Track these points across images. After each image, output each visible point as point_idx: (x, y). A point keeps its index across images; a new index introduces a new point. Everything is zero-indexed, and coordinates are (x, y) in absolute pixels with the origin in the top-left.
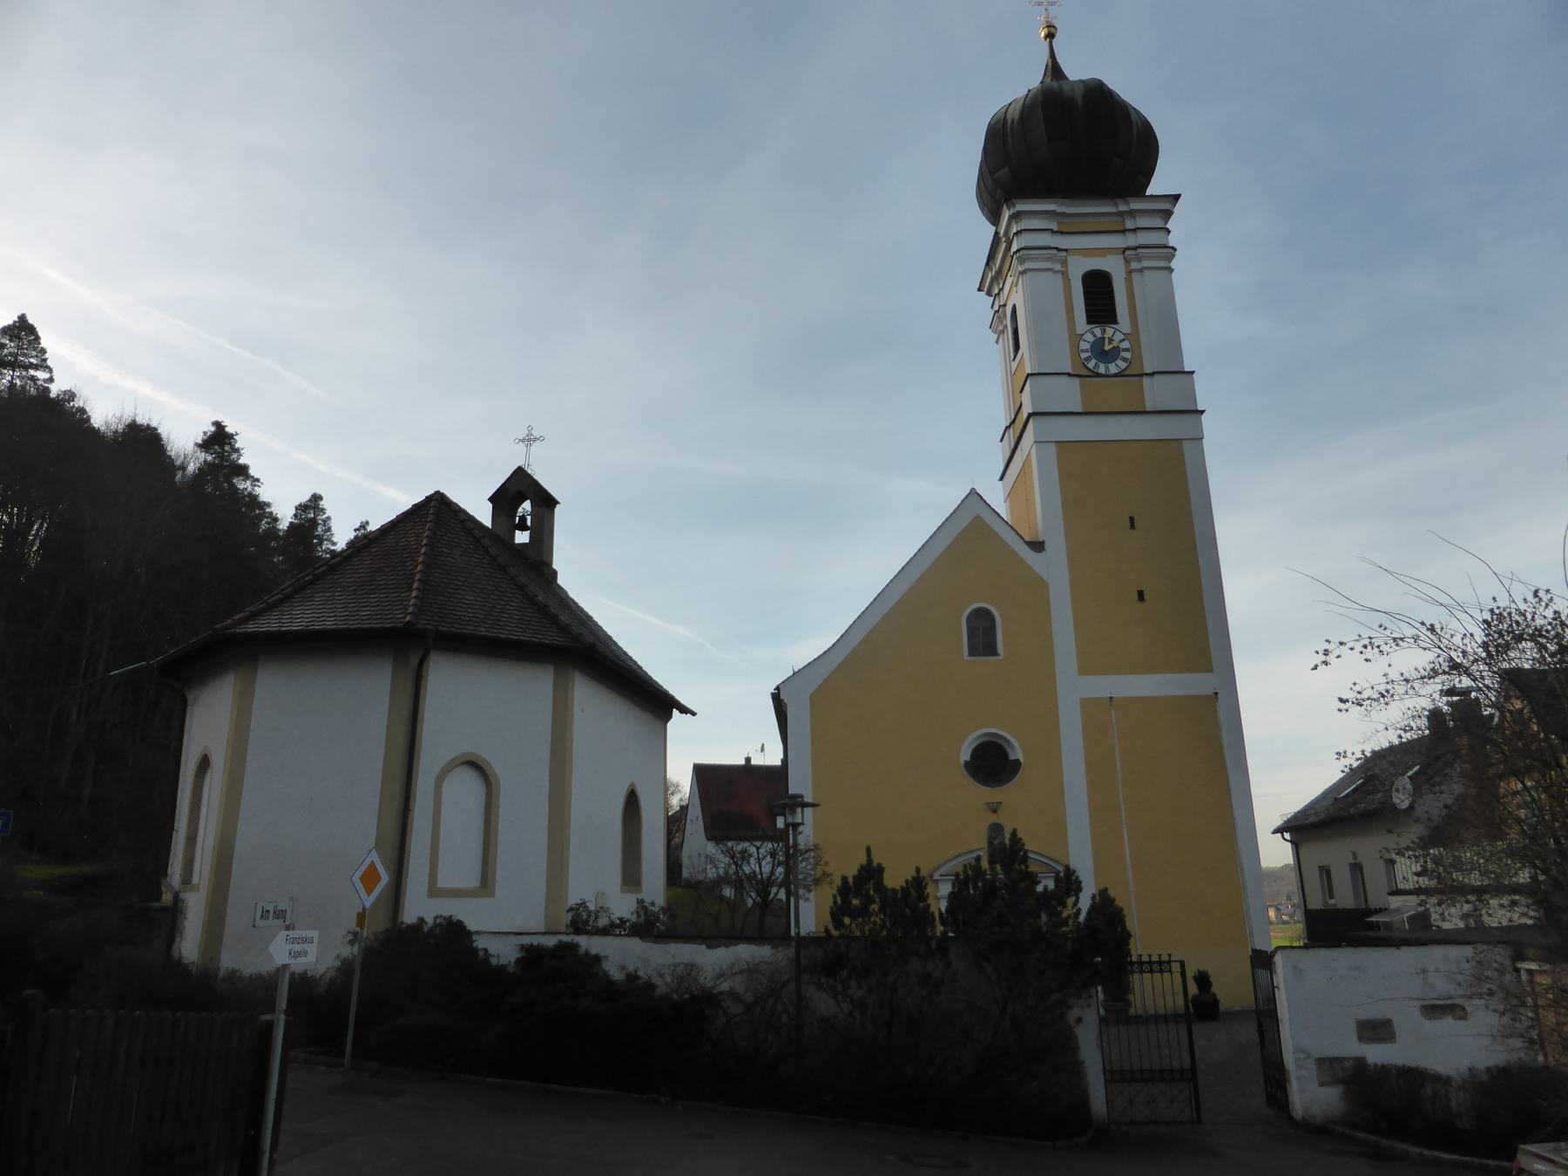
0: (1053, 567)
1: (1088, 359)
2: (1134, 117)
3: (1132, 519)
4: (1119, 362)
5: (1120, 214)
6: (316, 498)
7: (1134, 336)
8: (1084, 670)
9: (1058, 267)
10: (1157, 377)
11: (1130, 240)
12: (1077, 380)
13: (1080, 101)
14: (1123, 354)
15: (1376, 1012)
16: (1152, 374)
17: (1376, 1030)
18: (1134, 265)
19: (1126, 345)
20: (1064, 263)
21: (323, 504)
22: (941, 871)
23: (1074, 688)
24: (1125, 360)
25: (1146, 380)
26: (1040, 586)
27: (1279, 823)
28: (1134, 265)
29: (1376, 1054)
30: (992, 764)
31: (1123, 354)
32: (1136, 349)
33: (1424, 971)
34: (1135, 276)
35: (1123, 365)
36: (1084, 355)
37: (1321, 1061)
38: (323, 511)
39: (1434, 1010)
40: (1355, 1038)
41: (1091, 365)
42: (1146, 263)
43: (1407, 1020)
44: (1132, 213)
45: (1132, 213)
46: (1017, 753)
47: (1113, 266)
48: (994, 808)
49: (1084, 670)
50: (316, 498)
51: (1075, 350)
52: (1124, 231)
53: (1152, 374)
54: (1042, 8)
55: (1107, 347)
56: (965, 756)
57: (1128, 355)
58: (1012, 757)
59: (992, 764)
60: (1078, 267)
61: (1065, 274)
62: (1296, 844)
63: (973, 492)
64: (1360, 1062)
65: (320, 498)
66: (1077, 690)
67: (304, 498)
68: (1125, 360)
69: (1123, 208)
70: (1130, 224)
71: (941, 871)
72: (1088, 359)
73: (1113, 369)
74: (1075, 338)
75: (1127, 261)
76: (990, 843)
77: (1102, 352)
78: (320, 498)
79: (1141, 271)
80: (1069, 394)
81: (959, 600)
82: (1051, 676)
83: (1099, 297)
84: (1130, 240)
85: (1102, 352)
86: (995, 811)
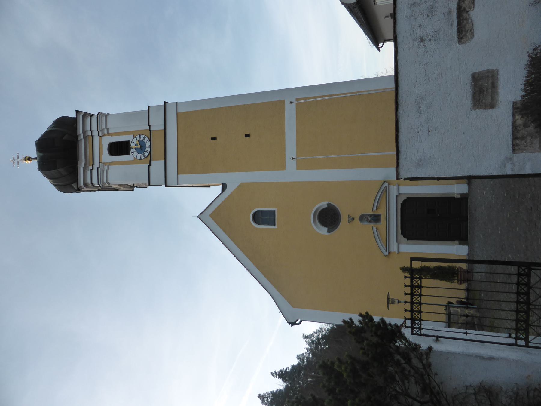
0: (235, 179)
1: (144, 155)
2: (50, 129)
3: (212, 139)
4: (145, 141)
5: (85, 137)
6: (259, 396)
7: (135, 133)
8: (282, 167)
9: (106, 167)
10: (150, 124)
11: (95, 133)
12: (152, 162)
13: (41, 154)
14: (142, 139)
15: (464, 91)
16: (150, 126)
17: (483, 88)
18: (106, 132)
19: (138, 137)
20: (105, 164)
21: (262, 394)
22: (384, 251)
23: (292, 173)
24: (144, 138)
25: (152, 129)
26: (242, 187)
27: (375, 48)
28: (106, 132)
29: (511, 89)
30: (329, 217)
31: (142, 139)
32: (140, 133)
33: (422, 40)
34: (110, 132)
35: (147, 139)
36: (143, 158)
37: (515, 148)
38: (264, 394)
39: (463, 30)
40: (491, 111)
41: (147, 154)
42: (104, 127)
43: (475, 57)
44: (84, 132)
45: (84, 132)
46: (324, 204)
47: (107, 141)
48: (351, 219)
49: (282, 167)
50: (259, 396)
51: (140, 161)
52: (92, 136)
53: (150, 126)
54: (20, 162)
55: (139, 147)
56: (323, 231)
57: (142, 136)
58: (326, 206)
59: (329, 217)
60: (107, 158)
61: (109, 164)
62: (385, 41)
63: (199, 217)
64: (519, 109)
65: (260, 395)
66: (293, 174)
67: (259, 401)
68: (144, 138)
69: (82, 137)
70: (89, 133)
71: (384, 251)
72: (144, 155)
73: (148, 144)
74: (135, 161)
75: (104, 135)
76: (370, 222)
77: (141, 148)
78: (260, 395)
79: (108, 129)
80: (157, 165)
81: (248, 228)
82: (285, 184)
83: (119, 149)
84: (95, 133)
85: (141, 148)
86: (353, 219)
